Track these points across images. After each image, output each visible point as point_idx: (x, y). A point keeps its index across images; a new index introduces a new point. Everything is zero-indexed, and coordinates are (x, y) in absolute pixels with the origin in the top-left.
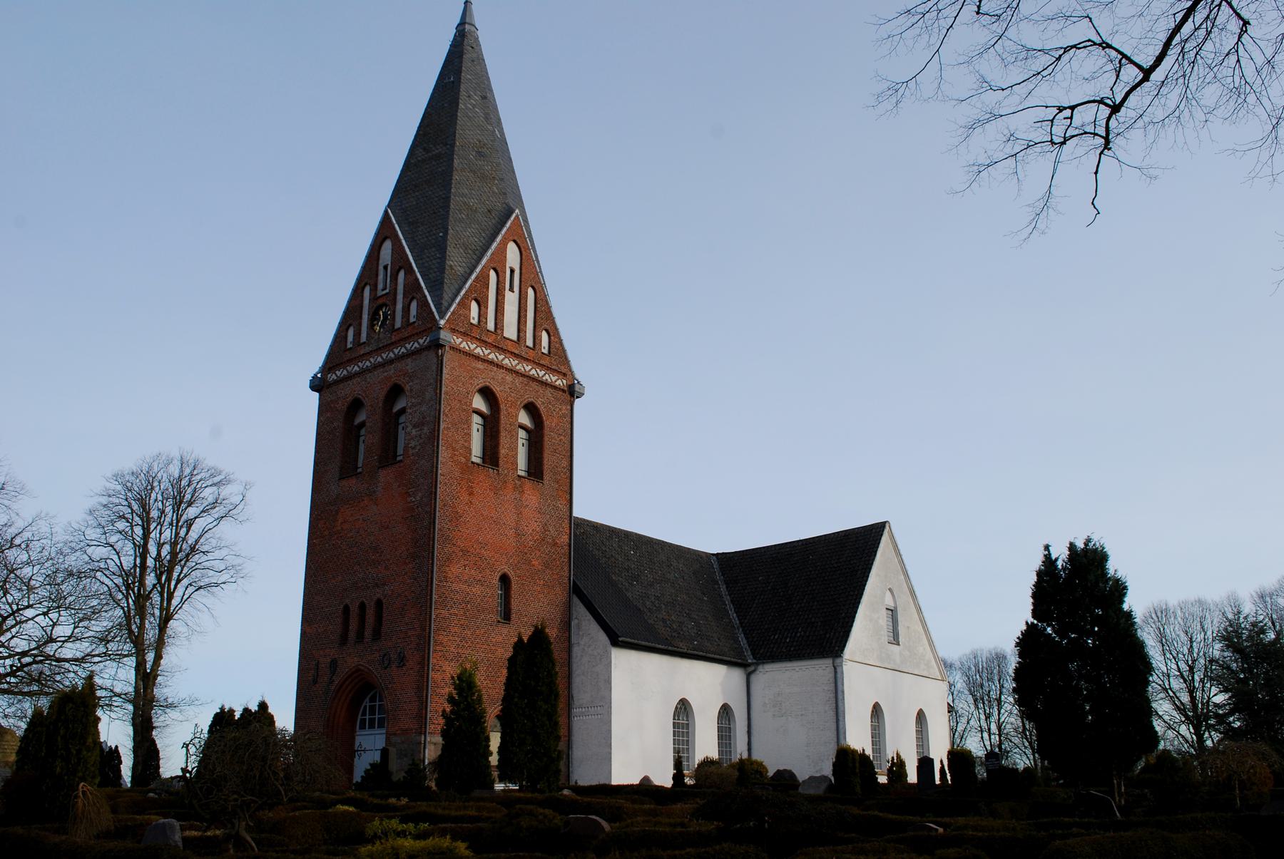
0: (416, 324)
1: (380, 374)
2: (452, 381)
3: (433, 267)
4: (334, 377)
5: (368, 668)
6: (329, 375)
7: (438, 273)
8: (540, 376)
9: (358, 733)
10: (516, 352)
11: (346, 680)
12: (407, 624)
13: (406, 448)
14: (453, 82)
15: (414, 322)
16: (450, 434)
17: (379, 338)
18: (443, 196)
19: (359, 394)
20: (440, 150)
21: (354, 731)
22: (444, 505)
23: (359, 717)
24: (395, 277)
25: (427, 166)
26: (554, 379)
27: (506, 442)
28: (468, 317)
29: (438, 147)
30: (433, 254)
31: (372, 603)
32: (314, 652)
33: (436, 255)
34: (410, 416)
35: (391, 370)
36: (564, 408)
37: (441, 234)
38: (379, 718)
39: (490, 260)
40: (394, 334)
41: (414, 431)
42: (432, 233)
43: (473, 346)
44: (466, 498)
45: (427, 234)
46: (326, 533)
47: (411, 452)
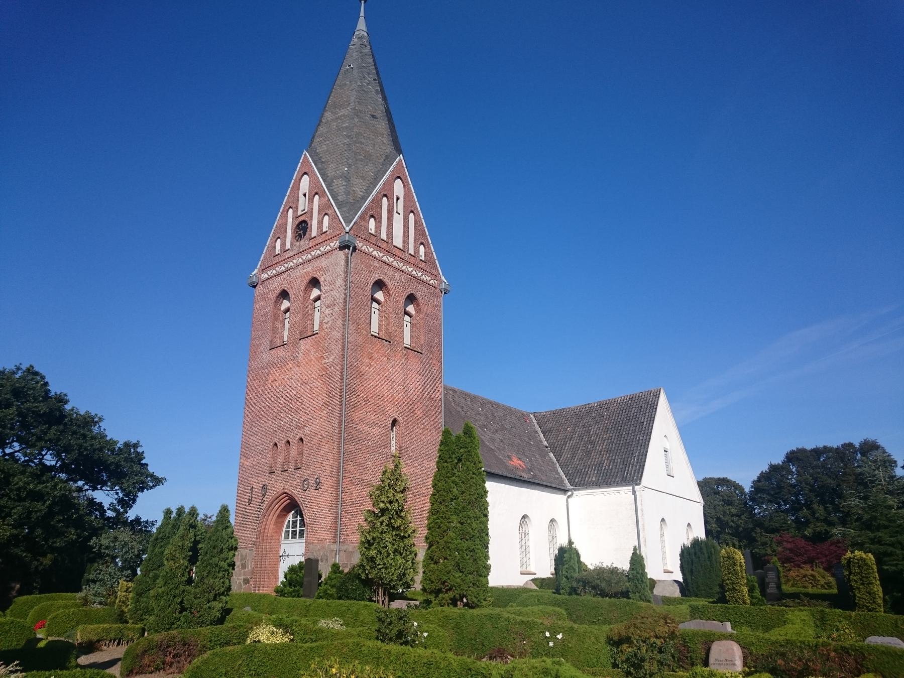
0: (328, 233)
1: (301, 271)
2: (357, 274)
3: (340, 191)
4: (266, 276)
5: (291, 491)
6: (263, 275)
7: (344, 196)
8: (419, 275)
9: (282, 542)
10: (402, 257)
11: (270, 506)
12: (322, 456)
13: (321, 323)
14: (352, 68)
15: (327, 231)
16: (355, 313)
17: (300, 245)
18: (347, 143)
19: (285, 287)
20: (344, 113)
21: (279, 540)
22: (351, 366)
23: (284, 529)
24: (311, 201)
25: (335, 124)
26: (429, 279)
27: (395, 321)
28: (367, 228)
29: (342, 111)
30: (340, 182)
31: (295, 441)
32: (249, 479)
33: (342, 183)
34: (324, 300)
35: (309, 268)
36: (436, 300)
37: (346, 169)
38: (296, 528)
39: (383, 188)
40: (311, 241)
41: (327, 310)
42: (339, 169)
43: (371, 250)
44: (367, 361)
45: (336, 170)
46: (260, 389)
47: (325, 326)
